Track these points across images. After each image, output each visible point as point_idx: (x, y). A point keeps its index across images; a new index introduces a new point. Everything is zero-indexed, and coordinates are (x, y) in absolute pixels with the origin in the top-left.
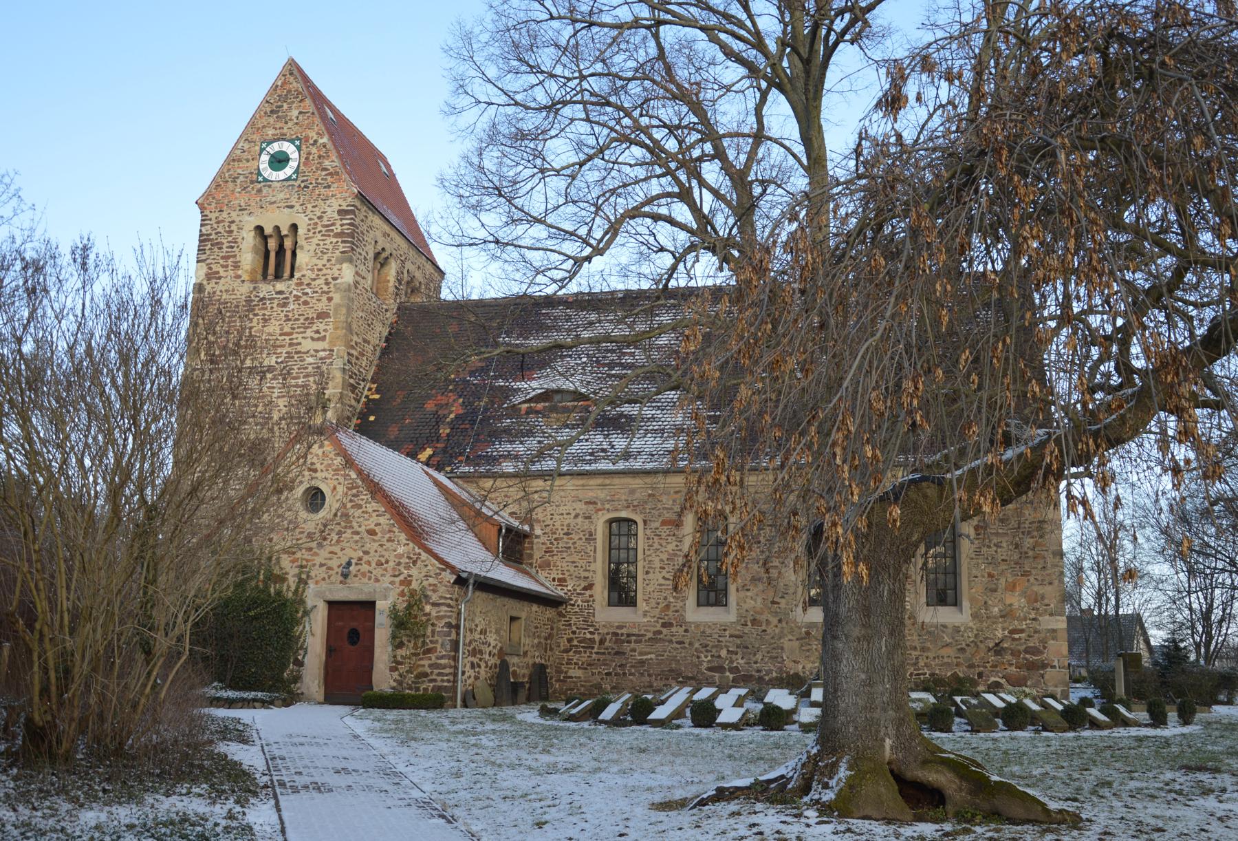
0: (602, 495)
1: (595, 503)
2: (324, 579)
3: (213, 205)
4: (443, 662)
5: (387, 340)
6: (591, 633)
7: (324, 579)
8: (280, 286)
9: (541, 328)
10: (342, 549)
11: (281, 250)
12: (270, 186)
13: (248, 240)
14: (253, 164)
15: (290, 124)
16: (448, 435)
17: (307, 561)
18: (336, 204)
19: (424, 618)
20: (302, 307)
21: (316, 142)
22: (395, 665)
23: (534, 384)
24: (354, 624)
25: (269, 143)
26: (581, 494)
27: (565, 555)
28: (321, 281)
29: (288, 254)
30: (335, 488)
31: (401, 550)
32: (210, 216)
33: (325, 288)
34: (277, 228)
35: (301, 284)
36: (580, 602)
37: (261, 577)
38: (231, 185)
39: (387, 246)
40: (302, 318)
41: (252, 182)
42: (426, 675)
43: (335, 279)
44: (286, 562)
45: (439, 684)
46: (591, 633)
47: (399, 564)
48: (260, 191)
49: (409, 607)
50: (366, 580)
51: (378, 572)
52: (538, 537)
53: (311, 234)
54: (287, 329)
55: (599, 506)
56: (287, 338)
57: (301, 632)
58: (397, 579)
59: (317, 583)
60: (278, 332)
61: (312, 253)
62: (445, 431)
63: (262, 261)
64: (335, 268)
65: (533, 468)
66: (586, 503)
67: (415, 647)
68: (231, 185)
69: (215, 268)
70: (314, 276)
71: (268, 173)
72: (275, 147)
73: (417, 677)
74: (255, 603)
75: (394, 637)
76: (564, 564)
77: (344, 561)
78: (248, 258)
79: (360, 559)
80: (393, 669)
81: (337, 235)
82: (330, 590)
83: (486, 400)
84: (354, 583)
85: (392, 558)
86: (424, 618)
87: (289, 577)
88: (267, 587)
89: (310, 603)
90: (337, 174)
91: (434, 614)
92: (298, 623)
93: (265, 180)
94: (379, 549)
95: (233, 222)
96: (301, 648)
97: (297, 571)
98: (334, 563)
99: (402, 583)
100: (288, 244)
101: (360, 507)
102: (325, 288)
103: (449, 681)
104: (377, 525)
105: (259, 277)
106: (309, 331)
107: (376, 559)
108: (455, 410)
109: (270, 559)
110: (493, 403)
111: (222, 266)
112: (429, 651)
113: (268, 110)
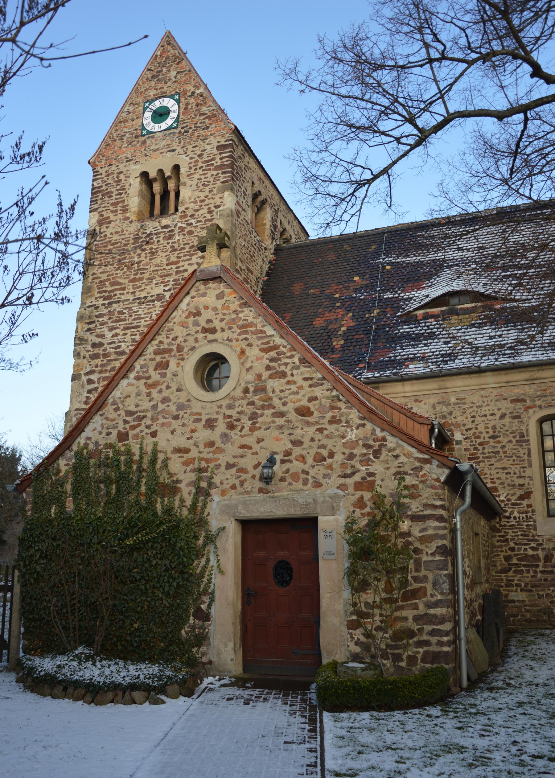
0: (530, 390)
1: (523, 400)
2: (234, 487)
3: (104, 161)
4: (438, 611)
5: (268, 274)
6: (533, 549)
7: (234, 487)
8: (165, 221)
9: (420, 247)
10: (259, 441)
11: (165, 194)
12: (153, 137)
13: (135, 185)
14: (138, 122)
15: (169, 84)
16: (342, 346)
17: (208, 461)
18: (214, 141)
19: (400, 542)
20: (187, 237)
21: (193, 93)
22: (358, 618)
23: (425, 292)
24: (282, 554)
25: (152, 101)
26: (505, 392)
27: (493, 461)
28: (205, 211)
29: (172, 195)
30: (243, 352)
31: (352, 435)
32: (101, 171)
33: (208, 216)
34: (161, 171)
35: (185, 216)
36: (516, 514)
37: (143, 489)
38: (118, 143)
39: (263, 191)
40: (187, 247)
41: (137, 137)
42: (411, 634)
43: (217, 207)
44: (176, 465)
45: (434, 648)
46: (533, 549)
47: (351, 457)
48: (144, 142)
49: (374, 524)
50: (299, 485)
51: (318, 471)
52: (459, 443)
53: (192, 171)
54: (173, 259)
55: (529, 403)
56: (174, 267)
57: (204, 568)
58: (350, 481)
59: (223, 493)
60: (165, 262)
61: (194, 187)
62: (338, 343)
63: (148, 207)
64: (217, 198)
65: (447, 367)
66: (513, 401)
67: (389, 589)
68: (118, 143)
69: (106, 214)
70: (197, 207)
71: (151, 126)
72: (157, 104)
73: (396, 636)
74: (133, 526)
75: (352, 573)
76: (494, 472)
77: (263, 458)
78: (134, 201)
79: (288, 453)
80: (352, 625)
81: (217, 168)
82: (244, 503)
83: (376, 311)
84: (283, 491)
85: (339, 449)
86: (400, 542)
87: (182, 486)
88: (151, 503)
89: (214, 524)
90: (214, 116)
91: (416, 532)
92: (199, 554)
93: (149, 132)
94: (318, 436)
95: (121, 172)
96: (205, 592)
97: (192, 476)
98: (248, 462)
99: (358, 486)
100: (171, 185)
101: (283, 375)
102: (208, 216)
103: (449, 643)
104: (310, 400)
105: (147, 214)
106: (194, 257)
107: (313, 452)
108: (347, 322)
109: (153, 461)
110: (385, 313)
111: (112, 212)
112: (415, 594)
113: (150, 76)
